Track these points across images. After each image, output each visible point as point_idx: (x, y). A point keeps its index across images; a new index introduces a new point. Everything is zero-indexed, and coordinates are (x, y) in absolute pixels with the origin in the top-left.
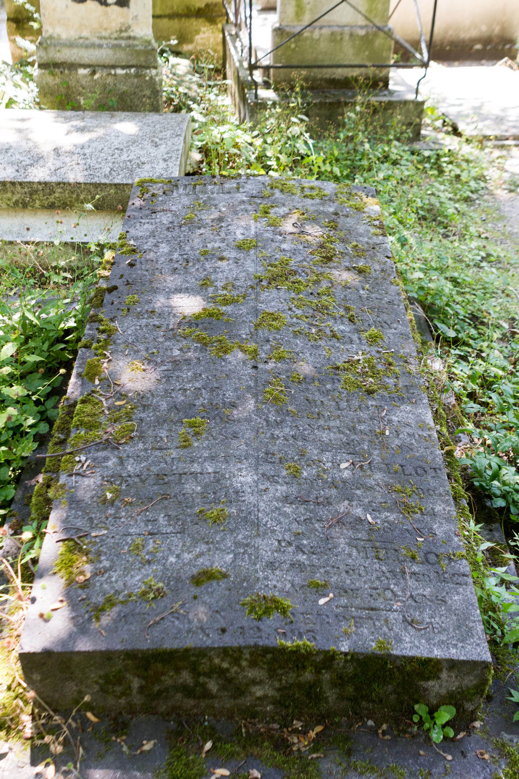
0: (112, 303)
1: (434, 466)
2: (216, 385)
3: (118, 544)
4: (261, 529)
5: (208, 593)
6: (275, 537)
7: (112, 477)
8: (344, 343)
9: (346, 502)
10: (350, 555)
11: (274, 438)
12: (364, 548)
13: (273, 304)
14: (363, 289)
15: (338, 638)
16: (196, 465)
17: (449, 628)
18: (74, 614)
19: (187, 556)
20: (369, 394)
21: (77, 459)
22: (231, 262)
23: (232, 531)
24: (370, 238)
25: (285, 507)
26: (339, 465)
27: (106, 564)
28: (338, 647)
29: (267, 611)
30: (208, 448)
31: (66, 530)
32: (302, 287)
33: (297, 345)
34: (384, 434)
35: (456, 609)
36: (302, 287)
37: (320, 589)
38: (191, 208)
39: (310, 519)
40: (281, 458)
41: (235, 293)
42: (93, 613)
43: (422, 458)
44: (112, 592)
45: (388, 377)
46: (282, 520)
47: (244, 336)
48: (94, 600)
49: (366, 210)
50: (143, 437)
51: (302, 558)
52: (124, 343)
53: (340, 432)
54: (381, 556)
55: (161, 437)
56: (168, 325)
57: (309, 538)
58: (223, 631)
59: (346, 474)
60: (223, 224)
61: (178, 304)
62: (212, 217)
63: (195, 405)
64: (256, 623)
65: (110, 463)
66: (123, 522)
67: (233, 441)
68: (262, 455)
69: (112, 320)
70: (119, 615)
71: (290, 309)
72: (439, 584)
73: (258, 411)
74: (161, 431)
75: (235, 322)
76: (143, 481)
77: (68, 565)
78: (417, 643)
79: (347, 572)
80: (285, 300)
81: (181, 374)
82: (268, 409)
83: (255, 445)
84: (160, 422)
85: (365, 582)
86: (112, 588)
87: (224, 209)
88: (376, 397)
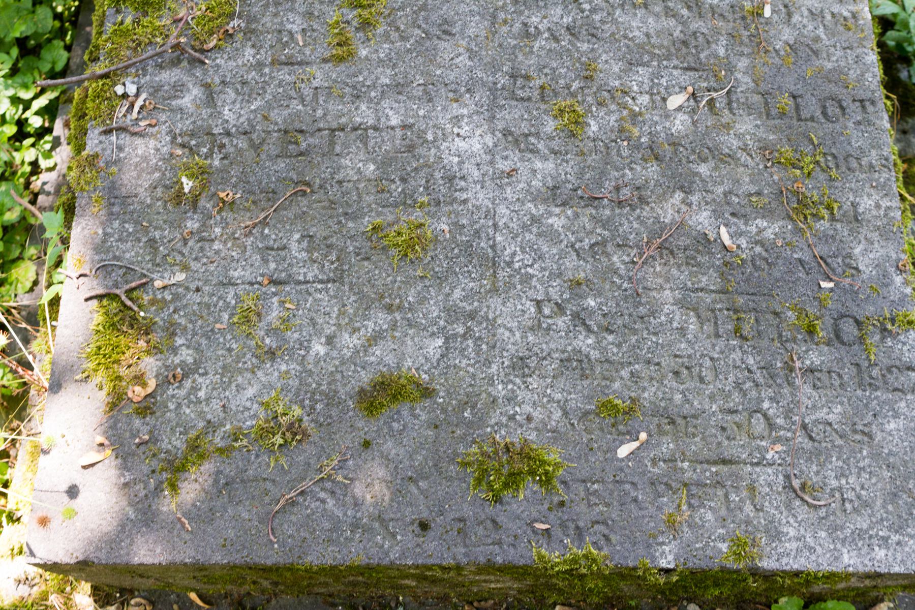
1: (861, 94)
3: (208, 306)
4: (501, 274)
5: (392, 433)
6: (530, 293)
7: (192, 135)
9: (678, 196)
10: (682, 331)
11: (528, 35)
12: (713, 311)
15: (655, 537)
16: (363, 107)
17: (874, 502)
18: (128, 477)
19: (349, 341)
21: (119, 90)
23: (440, 279)
25: (550, 214)
26: (664, 100)
27: (186, 355)
28: (653, 558)
29: (513, 480)
31: (103, 269)
34: (760, 15)
35: (891, 453)
37: (618, 416)
39: (603, 243)
40: (542, 88)
42: (165, 475)
43: (836, 76)
44: (201, 424)
46: (545, 248)
48: (165, 445)
50: (253, 31)
51: (585, 342)
54: (746, 330)
55: (290, 33)
57: (600, 294)
58: (424, 526)
59: (680, 124)
64: (490, 510)
65: (186, 101)
66: (217, 252)
67: (442, 45)
68: (503, 81)
70: (216, 481)
72: (859, 392)
74: (291, 16)
76: (256, 147)
77: (107, 356)
78: (810, 540)
79: (676, 373)
83: (488, 54)
85: (712, 398)
86: (201, 414)
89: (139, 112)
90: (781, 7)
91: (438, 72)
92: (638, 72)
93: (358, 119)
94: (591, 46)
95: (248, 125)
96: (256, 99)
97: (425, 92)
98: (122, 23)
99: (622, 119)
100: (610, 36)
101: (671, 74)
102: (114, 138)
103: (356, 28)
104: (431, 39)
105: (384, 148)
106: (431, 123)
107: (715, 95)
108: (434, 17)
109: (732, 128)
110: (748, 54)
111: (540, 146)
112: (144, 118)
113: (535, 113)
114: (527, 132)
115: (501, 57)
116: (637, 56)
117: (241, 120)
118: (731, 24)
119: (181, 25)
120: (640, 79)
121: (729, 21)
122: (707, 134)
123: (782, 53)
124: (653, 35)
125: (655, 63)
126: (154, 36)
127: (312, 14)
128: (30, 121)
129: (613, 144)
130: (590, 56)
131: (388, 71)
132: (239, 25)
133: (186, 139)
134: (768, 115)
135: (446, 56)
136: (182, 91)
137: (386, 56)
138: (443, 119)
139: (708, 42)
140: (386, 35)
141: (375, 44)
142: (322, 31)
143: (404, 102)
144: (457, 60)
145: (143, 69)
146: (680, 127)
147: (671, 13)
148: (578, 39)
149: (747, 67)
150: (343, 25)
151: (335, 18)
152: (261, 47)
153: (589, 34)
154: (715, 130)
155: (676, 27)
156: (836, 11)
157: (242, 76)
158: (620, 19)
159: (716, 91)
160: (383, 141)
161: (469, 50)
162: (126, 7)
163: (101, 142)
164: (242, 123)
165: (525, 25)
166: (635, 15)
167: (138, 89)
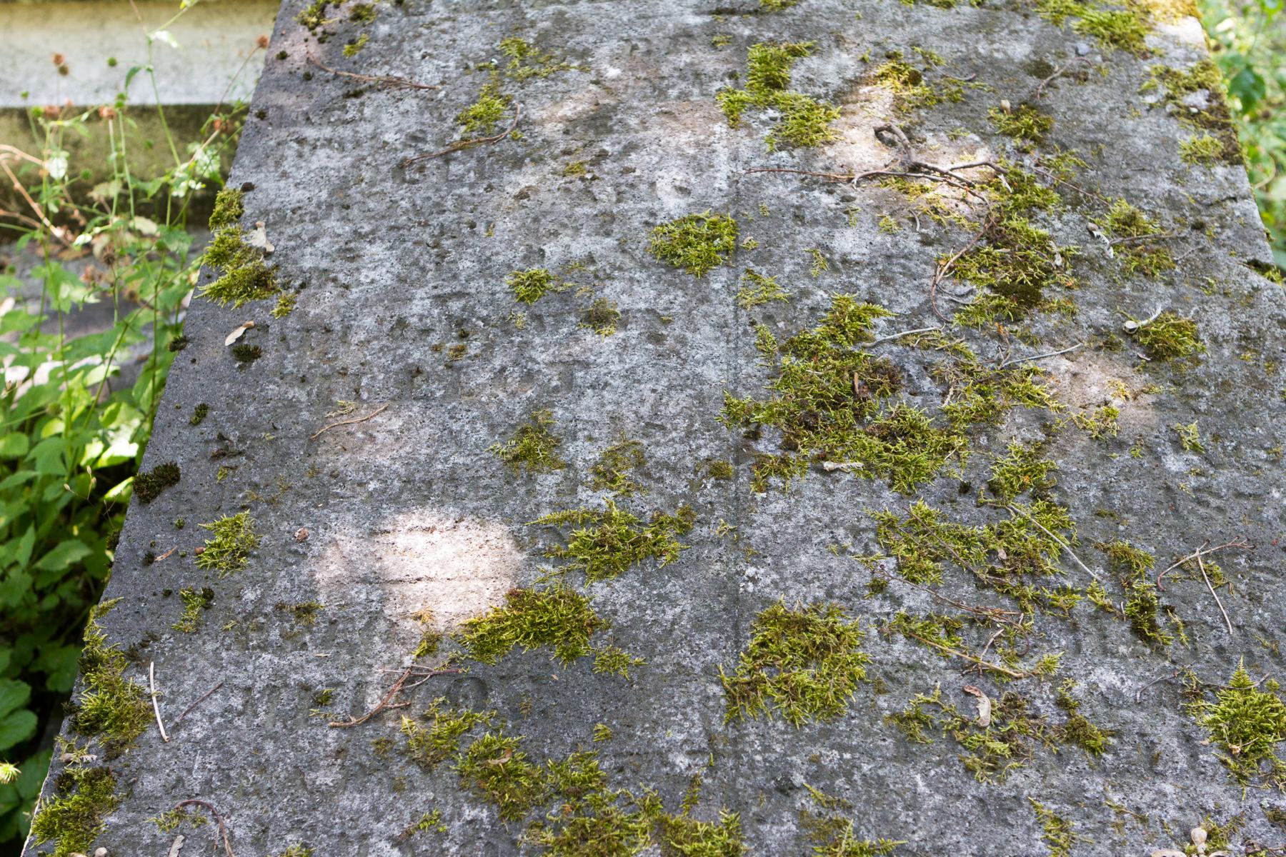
0: (150, 559)
8: (1120, 775)
14: (1178, 446)
22: (634, 332)
24: (1179, 177)
32: (922, 457)
36: (922, 457)
38: (489, 68)
41: (647, 503)
49: (1151, 41)
52: (169, 789)
56: (360, 685)
60: (606, 146)
61: (414, 566)
62: (568, 109)
69: (135, 658)
71: (878, 588)
80: (856, 532)
87: (613, 72)
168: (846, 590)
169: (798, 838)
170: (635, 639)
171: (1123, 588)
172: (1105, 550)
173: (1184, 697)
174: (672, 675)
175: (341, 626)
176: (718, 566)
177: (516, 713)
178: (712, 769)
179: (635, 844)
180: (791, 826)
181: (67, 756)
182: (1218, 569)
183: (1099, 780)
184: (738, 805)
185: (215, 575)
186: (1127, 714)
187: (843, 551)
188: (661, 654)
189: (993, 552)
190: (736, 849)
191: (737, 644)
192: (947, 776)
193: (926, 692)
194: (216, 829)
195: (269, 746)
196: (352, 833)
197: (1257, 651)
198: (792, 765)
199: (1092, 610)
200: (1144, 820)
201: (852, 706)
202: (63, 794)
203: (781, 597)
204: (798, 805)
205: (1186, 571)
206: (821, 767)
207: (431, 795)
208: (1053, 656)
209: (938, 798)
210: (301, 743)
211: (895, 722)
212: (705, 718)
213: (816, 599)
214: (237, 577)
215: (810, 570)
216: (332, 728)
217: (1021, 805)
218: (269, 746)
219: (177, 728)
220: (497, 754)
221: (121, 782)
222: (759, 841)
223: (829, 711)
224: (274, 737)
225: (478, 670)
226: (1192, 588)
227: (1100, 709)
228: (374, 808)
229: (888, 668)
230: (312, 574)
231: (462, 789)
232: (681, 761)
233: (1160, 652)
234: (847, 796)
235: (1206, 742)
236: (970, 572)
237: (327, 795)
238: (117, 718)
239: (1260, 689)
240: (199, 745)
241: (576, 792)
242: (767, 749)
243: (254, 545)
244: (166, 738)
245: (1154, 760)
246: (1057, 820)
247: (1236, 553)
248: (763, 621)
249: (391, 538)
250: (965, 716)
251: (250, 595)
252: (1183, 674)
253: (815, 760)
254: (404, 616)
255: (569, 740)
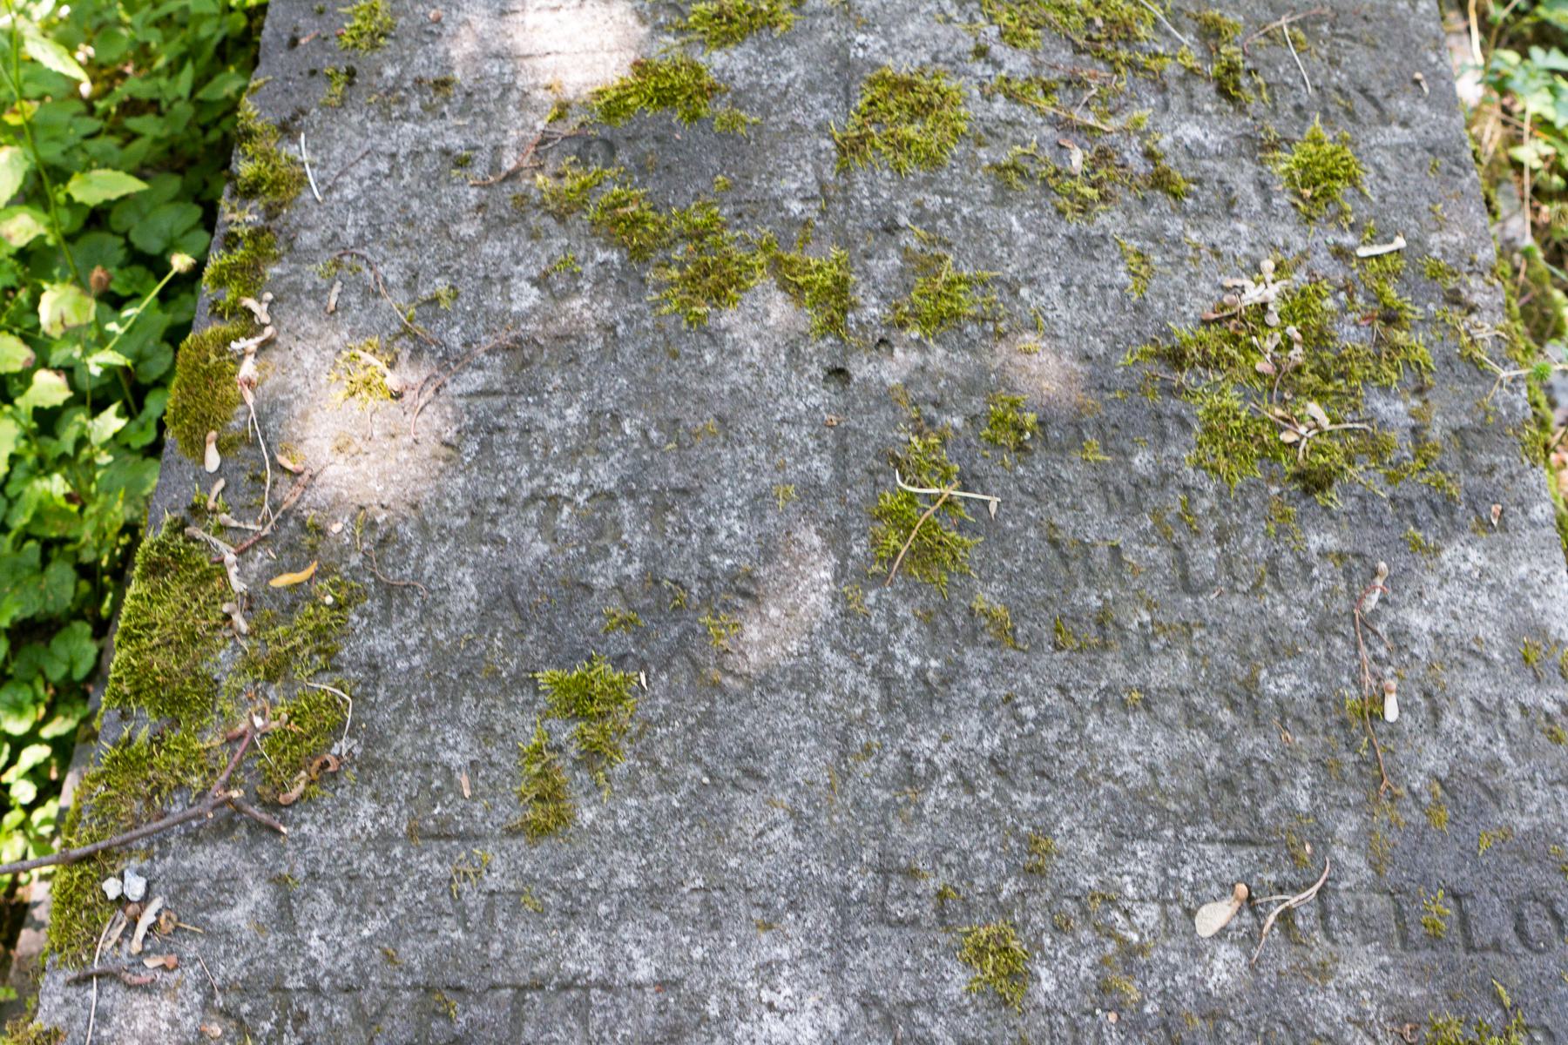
0: (294, 42)
2: (676, 478)
7: (245, 989)
8: (1199, 217)
13: (911, 28)
20: (1307, 492)
21: (112, 888)
26: (1190, 914)
30: (638, 839)
33: (1008, 241)
34: (1378, 717)
40: (941, 895)
45: (1385, 389)
47: (795, 207)
50: (375, 765)
52: (325, 244)
53: (1195, 718)
55: (447, 769)
56: (497, 149)
59: (1224, 970)
61: (540, 42)
63: (588, 589)
65: (238, 916)
67: (743, 801)
68: (862, 883)
69: (287, 130)
71: (981, 52)
73: (850, 627)
74: (450, 733)
75: (758, 128)
81: (541, 415)
82: (891, 616)
83: (833, 822)
84: (455, 674)
88: (1338, 505)
89: (146, 937)
90: (1419, 698)
91: (733, 863)
92: (1134, 853)
93: (571, 965)
94: (1039, 799)
95: (355, 972)
96: (373, 914)
97: (707, 905)
98: (130, 741)
99: (1104, 961)
100: (1077, 775)
101: (1202, 856)
102: (92, 994)
103: (575, 761)
104: (719, 789)
105: (621, 1032)
106: (717, 978)
107: (1293, 901)
108: (727, 740)
109: (1331, 975)
110: (1359, 805)
111: (936, 1031)
112: (157, 951)
113: (926, 953)
114: (910, 998)
115: (859, 829)
116: (1133, 817)
117: (342, 961)
118: (1321, 738)
119: (240, 749)
120: (1140, 869)
121: (1314, 732)
122: (1280, 990)
123: (1426, 799)
124: (1163, 769)
125: (1169, 833)
126: (187, 772)
127: (491, 729)
128: (13, 792)
129: (1088, 1019)
130: (1037, 820)
131: (634, 858)
132: (350, 751)
133: (233, 998)
134: (1404, 940)
135: (748, 828)
136: (231, 892)
137: (631, 825)
138: (742, 972)
139: (1275, 780)
140: (633, 778)
141: (611, 798)
142: (509, 766)
143: (665, 927)
144: (771, 837)
145: (161, 843)
146: (1225, 976)
147: (1199, 720)
148: (1012, 783)
149: (1356, 834)
150: (549, 756)
151: (534, 740)
152: (390, 799)
153: (1036, 772)
154: (1295, 982)
155: (1208, 749)
156: (1528, 702)
157: (349, 863)
158: (1097, 738)
159: (1296, 889)
160: (619, 1016)
161: (795, 814)
162: (140, 709)
163: (67, 1001)
164: (343, 968)
165: (906, 755)
166: (1127, 726)
167: (148, 885)
168: (950, 55)
169: (902, 270)
170: (752, 101)
171: (1211, 54)
172: (1196, 19)
173: (1263, 149)
174: (787, 132)
175: (476, 97)
176: (830, 35)
177: (642, 169)
178: (823, 213)
179: (753, 278)
180: (895, 260)
181: (230, 216)
182: (1301, 36)
183: (1179, 221)
184: (847, 243)
185: (356, 55)
186: (1208, 164)
187: (949, 20)
188: (776, 114)
189: (1090, 21)
190: (845, 280)
191: (848, 104)
192: (1040, 217)
193: (1024, 145)
194: (372, 276)
195: (415, 204)
196: (494, 276)
197: (1332, 108)
198: (897, 209)
199: (1181, 72)
200: (1218, 255)
201: (953, 157)
202: (229, 250)
203: (890, 61)
204: (902, 243)
205: (1272, 38)
206: (924, 210)
207: (566, 242)
208: (1142, 115)
209: (1031, 236)
210: (444, 200)
211: (994, 171)
212: (818, 170)
213: (922, 64)
214: (377, 56)
215: (917, 37)
216: (473, 186)
217: (1107, 242)
218: (415, 204)
219: (329, 190)
220: (625, 204)
221: (281, 238)
222: (867, 274)
223: (932, 161)
224: (420, 196)
225: (606, 132)
226: (1276, 53)
227: (1183, 160)
228: (514, 254)
229: (988, 125)
230: (447, 51)
231: (594, 235)
232: (795, 207)
233: (1242, 110)
234: (948, 234)
235: (1280, 188)
236: (1068, 38)
237: (471, 244)
238: (274, 182)
239: (1334, 141)
240: (350, 204)
241: (698, 235)
242: (874, 194)
243: (391, 27)
244: (320, 198)
245: (1230, 204)
246: (1139, 254)
247: (1319, 20)
248: (872, 83)
249: (520, 17)
250: (1059, 166)
251: (390, 72)
252: (1262, 128)
253: (919, 205)
254: (536, 87)
255: (692, 191)
